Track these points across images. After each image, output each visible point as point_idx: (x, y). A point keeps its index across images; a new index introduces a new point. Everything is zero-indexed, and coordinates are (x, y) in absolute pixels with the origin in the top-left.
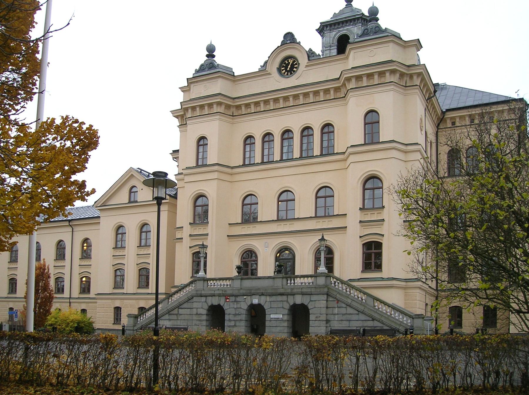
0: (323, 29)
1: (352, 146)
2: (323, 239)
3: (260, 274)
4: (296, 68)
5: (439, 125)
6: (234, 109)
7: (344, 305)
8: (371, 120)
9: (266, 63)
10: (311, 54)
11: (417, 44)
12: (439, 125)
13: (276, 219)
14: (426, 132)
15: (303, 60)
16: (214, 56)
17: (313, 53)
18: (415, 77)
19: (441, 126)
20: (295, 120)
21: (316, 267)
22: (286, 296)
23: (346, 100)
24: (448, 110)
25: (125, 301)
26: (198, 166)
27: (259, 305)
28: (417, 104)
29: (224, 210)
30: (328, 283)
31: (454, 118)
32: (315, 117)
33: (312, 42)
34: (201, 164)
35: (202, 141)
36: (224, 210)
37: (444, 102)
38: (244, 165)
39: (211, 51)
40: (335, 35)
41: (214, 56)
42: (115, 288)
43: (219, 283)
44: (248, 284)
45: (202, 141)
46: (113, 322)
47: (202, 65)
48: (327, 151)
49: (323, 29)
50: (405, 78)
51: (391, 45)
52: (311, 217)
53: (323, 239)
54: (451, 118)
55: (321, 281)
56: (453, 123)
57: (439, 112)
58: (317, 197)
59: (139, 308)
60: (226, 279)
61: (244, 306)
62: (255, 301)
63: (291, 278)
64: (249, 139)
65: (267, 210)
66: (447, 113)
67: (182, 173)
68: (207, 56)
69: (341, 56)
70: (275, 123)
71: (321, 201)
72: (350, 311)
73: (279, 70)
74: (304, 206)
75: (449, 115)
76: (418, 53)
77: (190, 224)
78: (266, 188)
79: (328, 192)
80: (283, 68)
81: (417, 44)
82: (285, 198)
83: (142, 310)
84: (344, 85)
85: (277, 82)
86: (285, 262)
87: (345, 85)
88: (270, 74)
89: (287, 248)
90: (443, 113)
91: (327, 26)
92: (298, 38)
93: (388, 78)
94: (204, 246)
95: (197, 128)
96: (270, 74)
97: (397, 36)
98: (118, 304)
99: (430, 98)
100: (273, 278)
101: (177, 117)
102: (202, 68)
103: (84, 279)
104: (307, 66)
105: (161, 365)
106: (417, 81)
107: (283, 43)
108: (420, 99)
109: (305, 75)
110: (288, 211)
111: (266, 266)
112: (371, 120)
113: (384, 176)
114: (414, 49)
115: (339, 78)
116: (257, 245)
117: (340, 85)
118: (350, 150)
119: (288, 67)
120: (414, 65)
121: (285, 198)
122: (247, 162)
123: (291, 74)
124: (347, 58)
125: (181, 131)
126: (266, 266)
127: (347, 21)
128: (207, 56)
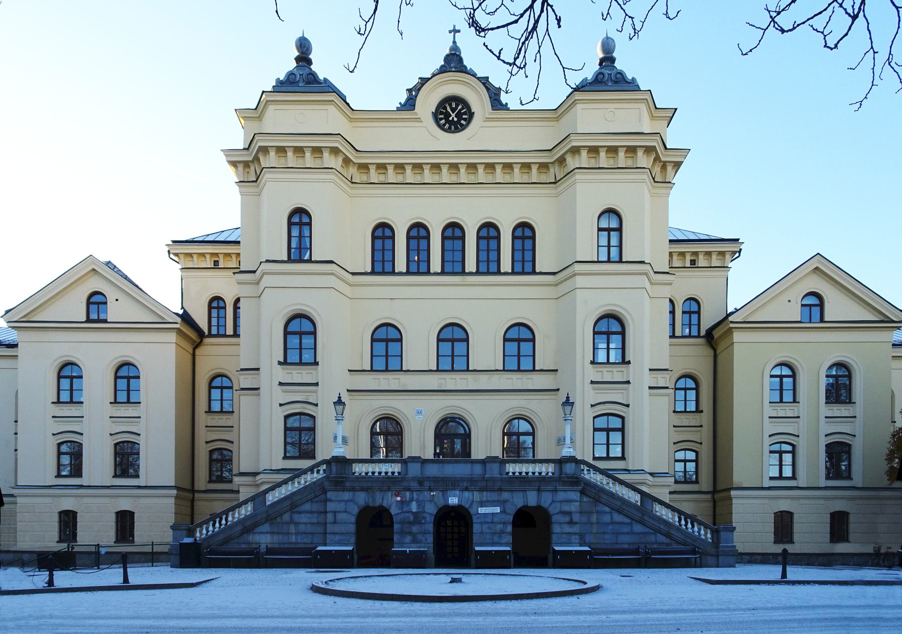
1: (268, 261)
3: (473, 457)
4: (465, 119)
6: (356, 170)
7: (607, 509)
20: (471, 209)
23: (258, 186)
25: (86, 500)
27: (539, 509)
29: (343, 346)
32: (506, 209)
35: (300, 218)
36: (343, 346)
39: (304, 50)
46: (57, 539)
50: (552, 170)
51: (331, 108)
52: (431, 371)
61: (431, 509)
62: (453, 501)
64: (382, 233)
70: (436, 209)
72: (618, 518)
73: (435, 115)
77: (280, 363)
78: (421, 306)
80: (442, 116)
82: (453, 337)
85: (424, 136)
87: (258, 160)
95: (284, 192)
96: (418, 120)
98: (125, 505)
101: (234, 164)
104: (488, 119)
105: (384, 612)
107: (442, 70)
110: (521, 358)
112: (612, 222)
113: (632, 318)
116: (401, 407)
117: (355, 161)
118: (578, 268)
121: (453, 337)
123: (456, 128)
125: (242, 194)
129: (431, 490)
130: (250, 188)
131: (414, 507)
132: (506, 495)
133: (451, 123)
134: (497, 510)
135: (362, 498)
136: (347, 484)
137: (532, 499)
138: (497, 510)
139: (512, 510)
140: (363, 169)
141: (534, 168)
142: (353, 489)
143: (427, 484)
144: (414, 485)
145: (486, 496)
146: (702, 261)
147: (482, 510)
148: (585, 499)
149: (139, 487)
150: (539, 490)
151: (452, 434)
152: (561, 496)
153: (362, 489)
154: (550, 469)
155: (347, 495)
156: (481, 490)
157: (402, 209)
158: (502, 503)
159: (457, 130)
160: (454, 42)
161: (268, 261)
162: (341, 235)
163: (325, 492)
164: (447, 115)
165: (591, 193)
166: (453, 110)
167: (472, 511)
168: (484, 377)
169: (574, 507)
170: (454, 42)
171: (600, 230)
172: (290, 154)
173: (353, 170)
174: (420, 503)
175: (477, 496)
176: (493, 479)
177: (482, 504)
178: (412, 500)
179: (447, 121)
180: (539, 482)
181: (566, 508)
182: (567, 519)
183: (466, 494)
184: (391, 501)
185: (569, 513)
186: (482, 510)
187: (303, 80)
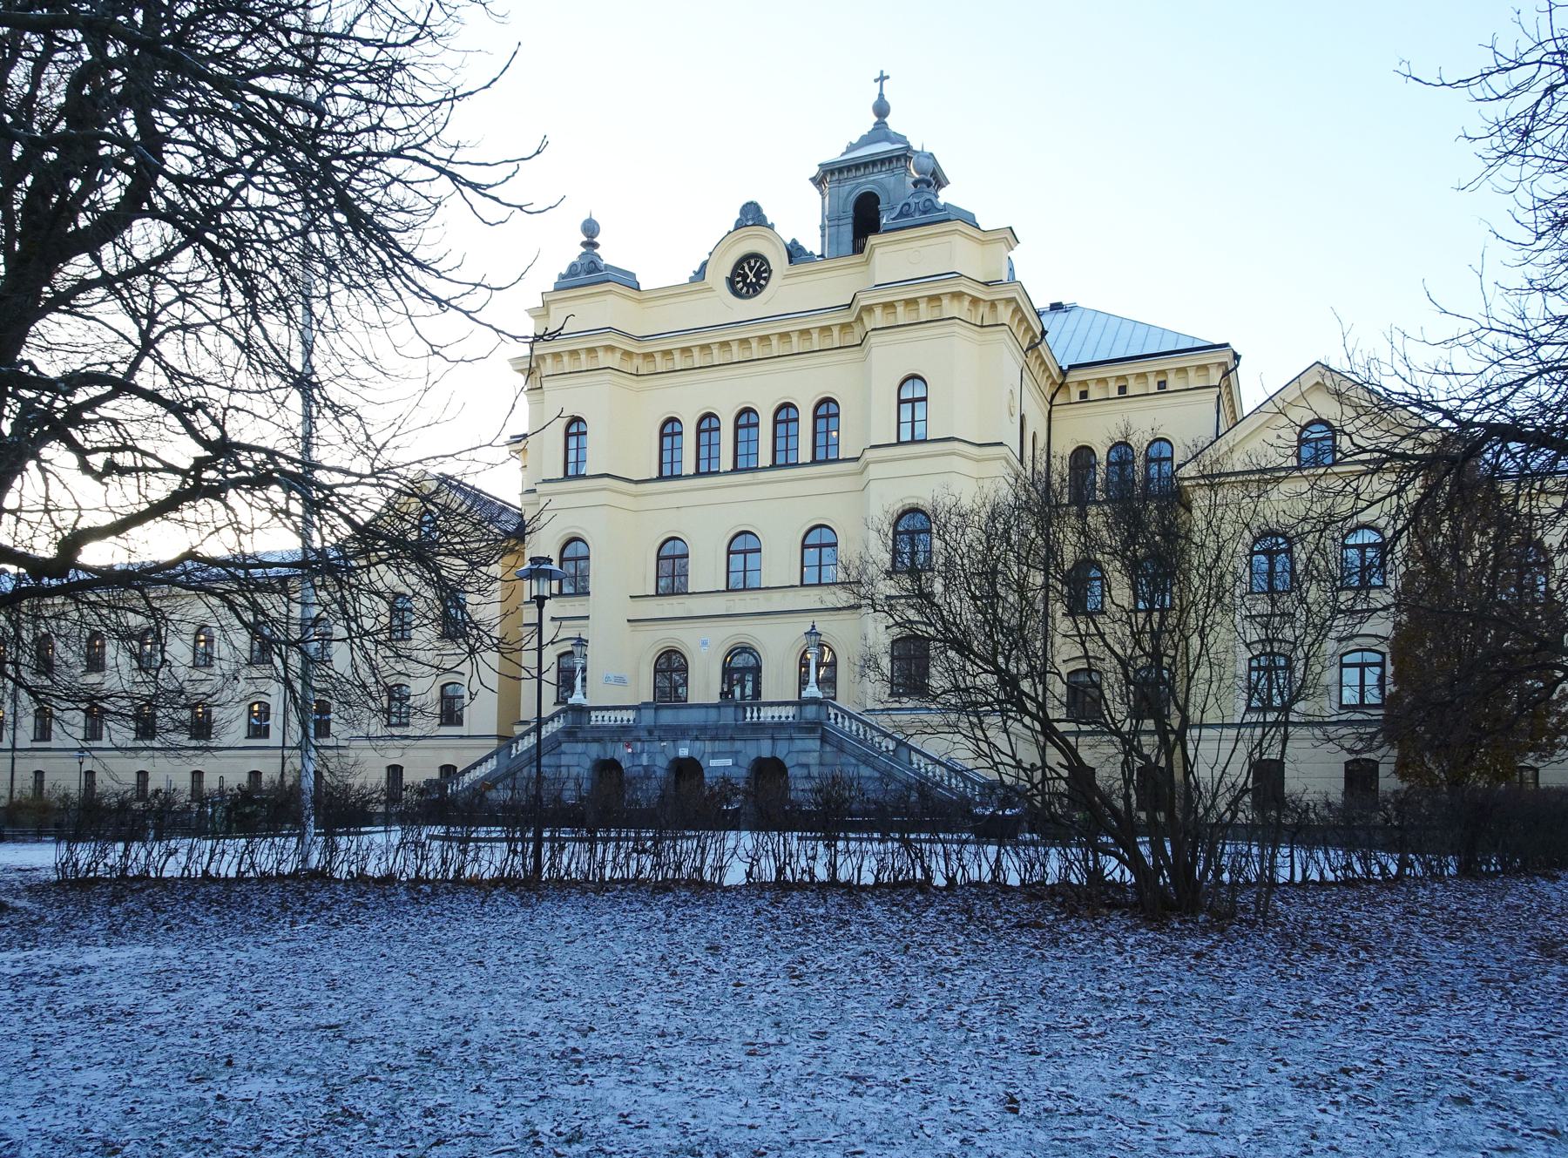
0: (824, 177)
2: (812, 633)
5: (1053, 396)
8: (912, 392)
9: (704, 265)
10: (795, 253)
11: (1010, 237)
12: (1053, 396)
13: (723, 588)
14: (1022, 418)
15: (778, 261)
16: (596, 245)
17: (801, 249)
18: (1001, 307)
19: (1057, 400)
20: (762, 389)
21: (803, 683)
22: (415, 255)
24: (1071, 367)
26: (567, 477)
28: (1005, 355)
29: (620, 570)
30: (824, 716)
31: (1084, 383)
32: (802, 384)
33: (801, 217)
34: (572, 473)
35: (575, 427)
36: (620, 570)
37: (1065, 346)
38: (661, 478)
40: (850, 193)
41: (596, 245)
42: (35, 740)
43: (613, 714)
44: (667, 717)
45: (575, 427)
47: (573, 265)
48: (824, 455)
49: (824, 177)
53: (812, 633)
54: (1080, 383)
55: (810, 712)
56: (1084, 395)
57: (1055, 372)
58: (804, 546)
59: (442, 768)
60: (626, 708)
61: (662, 762)
62: (684, 752)
63: (751, 705)
64: (670, 428)
65: (706, 568)
66: (1071, 373)
67: (534, 491)
68: (584, 244)
69: (858, 258)
70: (723, 394)
71: (812, 554)
73: (731, 282)
74: (780, 561)
75: (1075, 376)
76: (1011, 254)
78: (705, 515)
79: (827, 537)
81: (1010, 237)
82: (743, 546)
83: (448, 775)
84: (859, 319)
86: (741, 669)
88: (710, 289)
89: (745, 649)
90: (1064, 373)
91: (832, 172)
92: (767, 212)
93: (950, 308)
94: (581, 642)
96: (710, 289)
97: (969, 219)
99: (1033, 346)
100: (717, 706)
102: (573, 270)
103: (256, 708)
104: (786, 277)
106: (1005, 314)
107: (739, 225)
108: (1011, 352)
109: (785, 293)
111: (704, 685)
112: (912, 392)
114: (1003, 246)
115: (850, 305)
116: (688, 639)
118: (870, 454)
119: (748, 276)
120: (999, 282)
121: (743, 546)
122: (667, 472)
123: (755, 291)
124: (867, 262)
126: (704, 685)
127: (874, 163)
128: (584, 244)
129: (661, 740)
130: (536, 395)
131: (645, 760)
132: (738, 745)
133: (749, 285)
134: (729, 762)
135: (595, 750)
136: (580, 735)
137: (765, 749)
138: (729, 762)
139: (745, 762)
140: (647, 357)
141: (836, 331)
142: (585, 741)
143: (656, 733)
144: (643, 735)
145: (718, 746)
146: (1173, 383)
147: (713, 763)
148: (828, 748)
149: (461, 737)
150: (773, 738)
151: (741, 669)
152: (799, 745)
153: (595, 740)
154: (790, 711)
155: (580, 747)
156: (713, 739)
157: (688, 398)
158: (734, 754)
159: (756, 293)
160: (881, 95)
161: (545, 481)
162: (625, 442)
163: (560, 744)
164: (745, 276)
165: (891, 357)
166: (751, 269)
167: (703, 764)
168: (776, 595)
169: (812, 759)
170: (881, 95)
171: (900, 402)
172: (566, 358)
173: (638, 361)
174: (651, 755)
175: (709, 746)
176: (725, 727)
177: (714, 755)
178: (642, 752)
179: (745, 284)
180: (776, 730)
181: (804, 759)
182: (804, 772)
183: (698, 744)
184: (622, 753)
185: (807, 766)
186: (713, 763)
187: (588, 272)
